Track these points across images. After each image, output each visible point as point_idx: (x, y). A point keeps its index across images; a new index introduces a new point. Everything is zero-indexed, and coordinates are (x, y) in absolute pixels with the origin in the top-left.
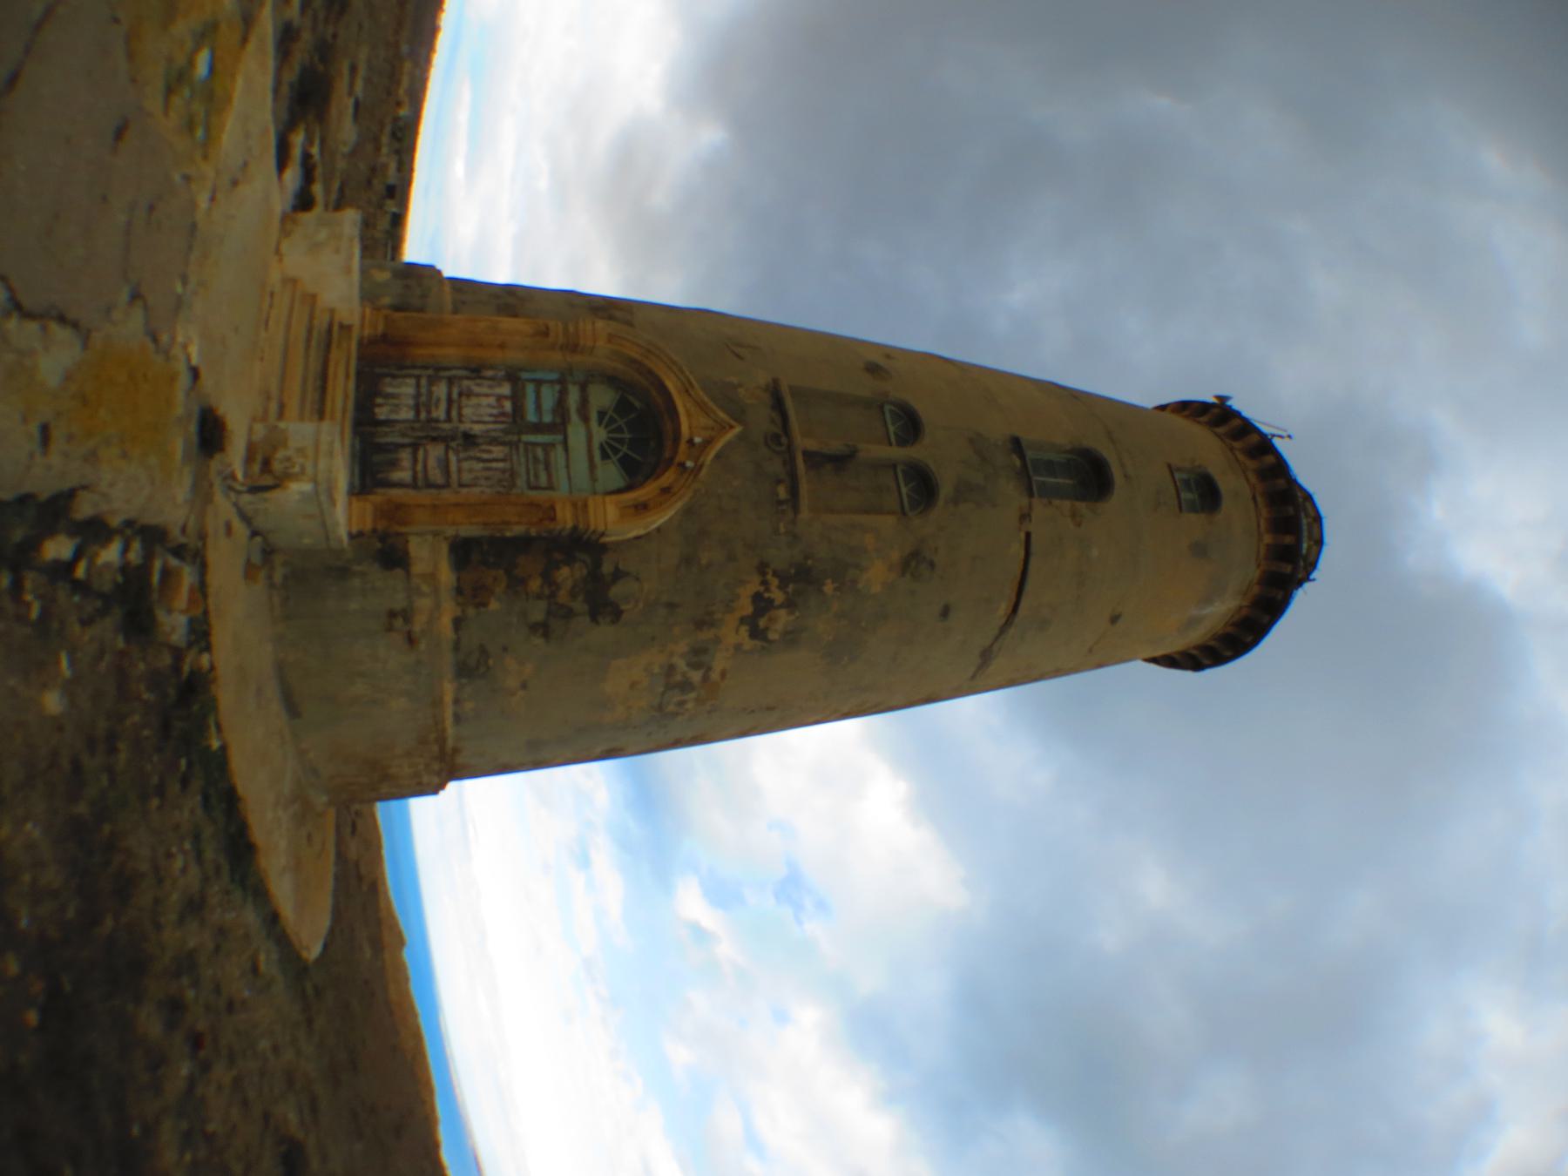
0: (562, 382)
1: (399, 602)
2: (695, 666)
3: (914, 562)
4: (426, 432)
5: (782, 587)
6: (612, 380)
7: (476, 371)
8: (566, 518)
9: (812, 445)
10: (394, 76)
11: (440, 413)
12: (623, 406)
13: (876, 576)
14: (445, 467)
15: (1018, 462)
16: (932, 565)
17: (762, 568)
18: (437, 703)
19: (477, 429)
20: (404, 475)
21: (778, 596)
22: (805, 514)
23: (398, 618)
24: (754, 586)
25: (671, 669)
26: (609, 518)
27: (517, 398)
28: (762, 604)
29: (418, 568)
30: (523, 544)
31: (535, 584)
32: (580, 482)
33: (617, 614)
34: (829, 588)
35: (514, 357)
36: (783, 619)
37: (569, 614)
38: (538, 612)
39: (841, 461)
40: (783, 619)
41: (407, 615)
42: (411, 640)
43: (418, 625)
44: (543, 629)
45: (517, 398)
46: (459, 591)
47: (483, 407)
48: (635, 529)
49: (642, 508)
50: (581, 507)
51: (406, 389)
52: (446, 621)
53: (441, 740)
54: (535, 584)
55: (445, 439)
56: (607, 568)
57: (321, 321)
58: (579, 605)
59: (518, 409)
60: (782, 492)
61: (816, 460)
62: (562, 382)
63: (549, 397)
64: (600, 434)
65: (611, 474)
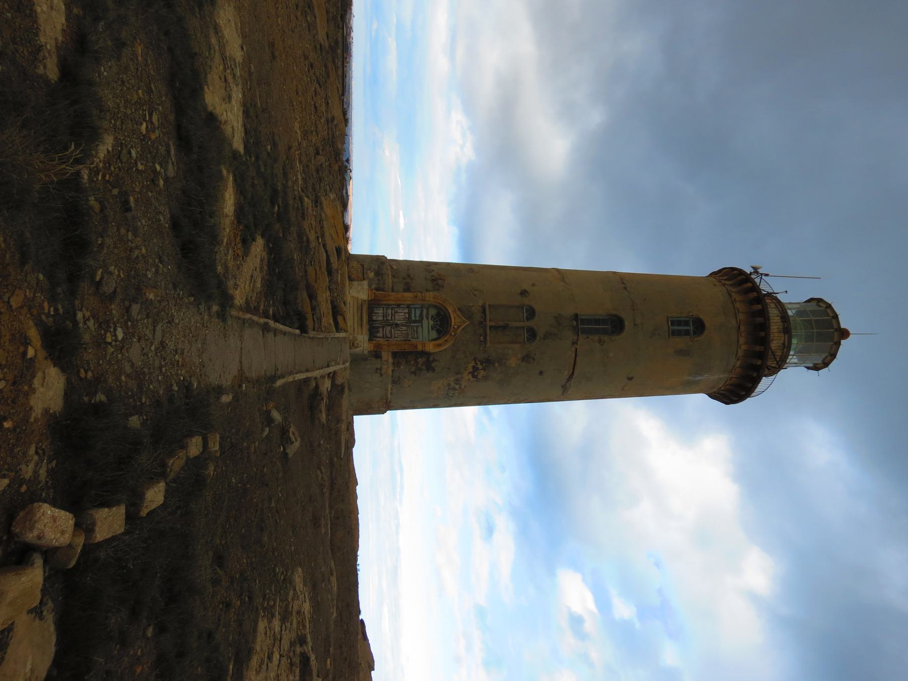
0: (422, 307)
1: (379, 366)
4: (386, 323)
5: (481, 364)
6: (435, 307)
8: (420, 348)
9: (493, 324)
11: (389, 318)
12: (438, 314)
13: (513, 362)
15: (575, 324)
16: (534, 359)
17: (475, 359)
18: (387, 390)
19: (399, 322)
20: (380, 335)
21: (480, 367)
22: (488, 344)
23: (379, 370)
24: (473, 364)
25: (449, 385)
26: (430, 348)
27: (409, 313)
28: (475, 369)
29: (384, 359)
30: (410, 353)
31: (413, 362)
32: (425, 337)
33: (434, 370)
34: (496, 365)
35: (408, 302)
36: (482, 373)
37: (421, 370)
38: (413, 369)
40: (482, 373)
41: (381, 369)
42: (381, 375)
43: (383, 371)
44: (414, 373)
45: (409, 313)
47: (400, 317)
48: (437, 350)
49: (439, 345)
50: (424, 345)
51: (380, 311)
52: (390, 372)
53: (387, 399)
54: (413, 362)
55: (391, 325)
56: (431, 359)
57: (360, 302)
58: (424, 368)
60: (482, 338)
62: (422, 307)
64: (431, 323)
65: (434, 334)
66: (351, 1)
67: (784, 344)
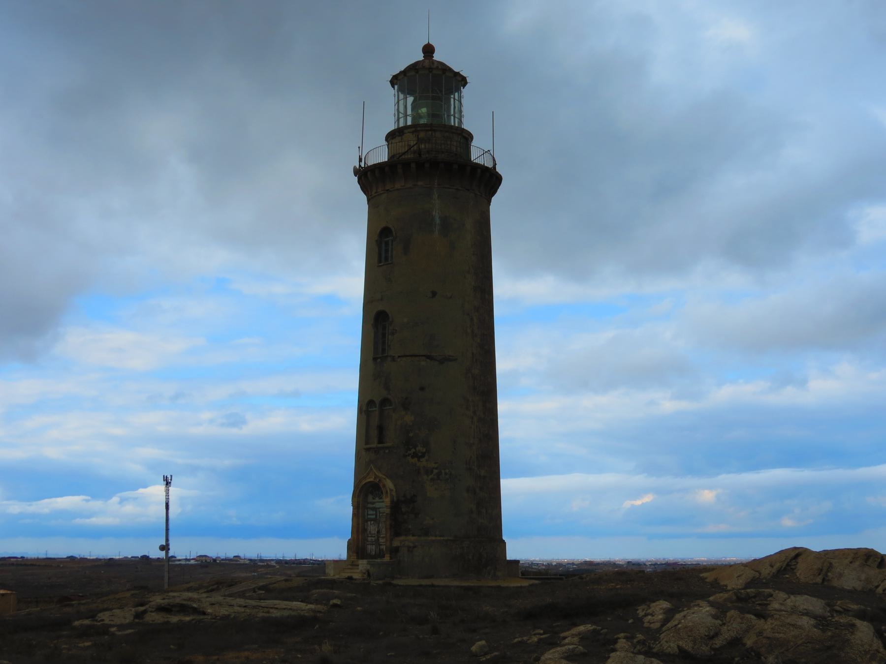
2: (432, 472)
21: (413, 450)
24: (409, 458)
25: (432, 479)
27: (371, 520)
28: (415, 455)
34: (411, 435)
40: (420, 448)
42: (415, 547)
43: (411, 545)
45: (371, 520)
46: (406, 535)
51: (369, 547)
55: (378, 537)
61: (381, 441)
63: (371, 512)
66: (4, 559)
67: (413, 132)
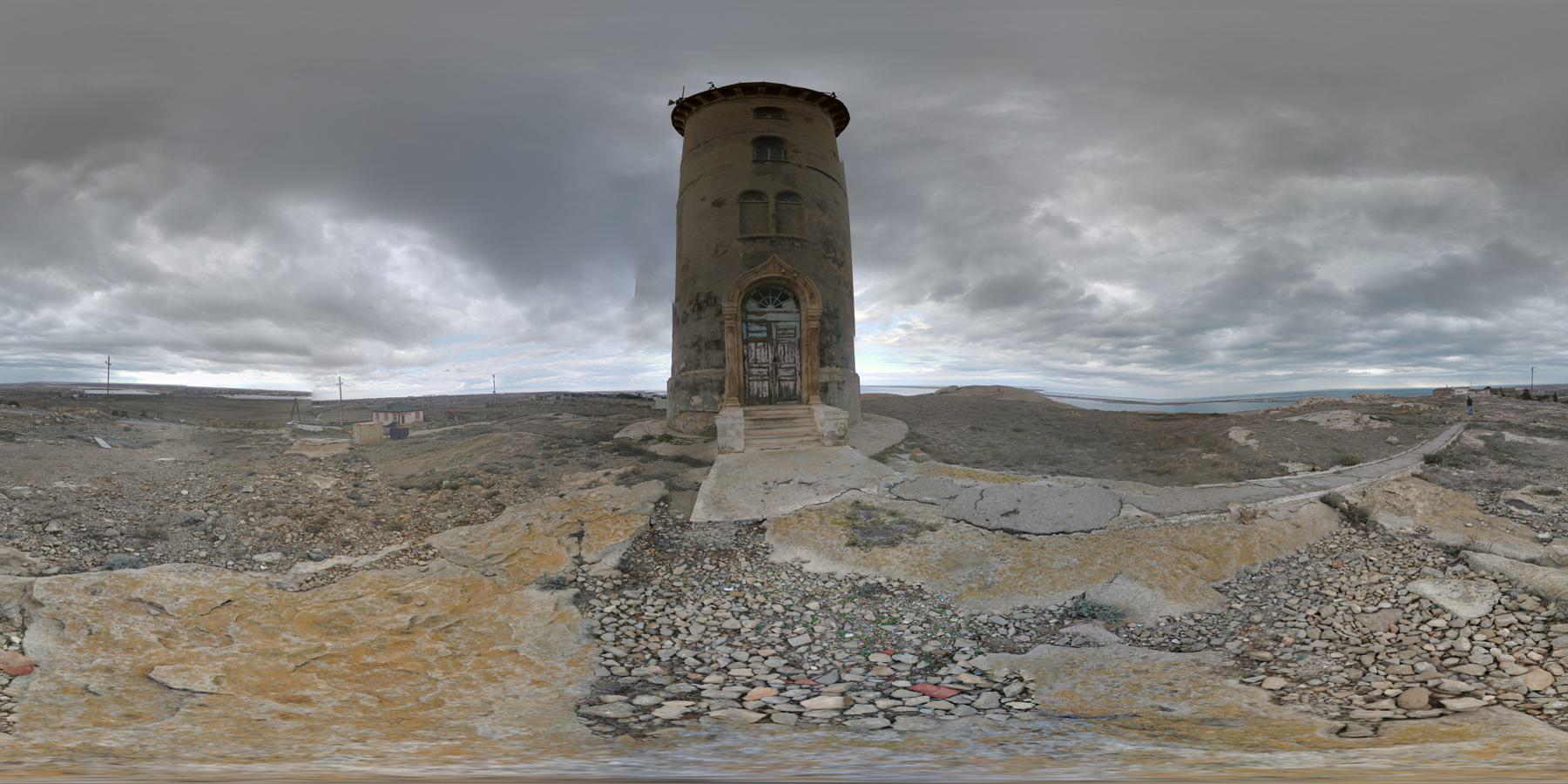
3: (822, 206)
4: (773, 376)
7: (745, 357)
10: (170, 397)
12: (756, 298)
14: (787, 369)
27: (756, 340)
39: (778, 222)
45: (756, 340)
47: (762, 354)
49: (812, 296)
59: (761, 340)
64: (771, 307)
